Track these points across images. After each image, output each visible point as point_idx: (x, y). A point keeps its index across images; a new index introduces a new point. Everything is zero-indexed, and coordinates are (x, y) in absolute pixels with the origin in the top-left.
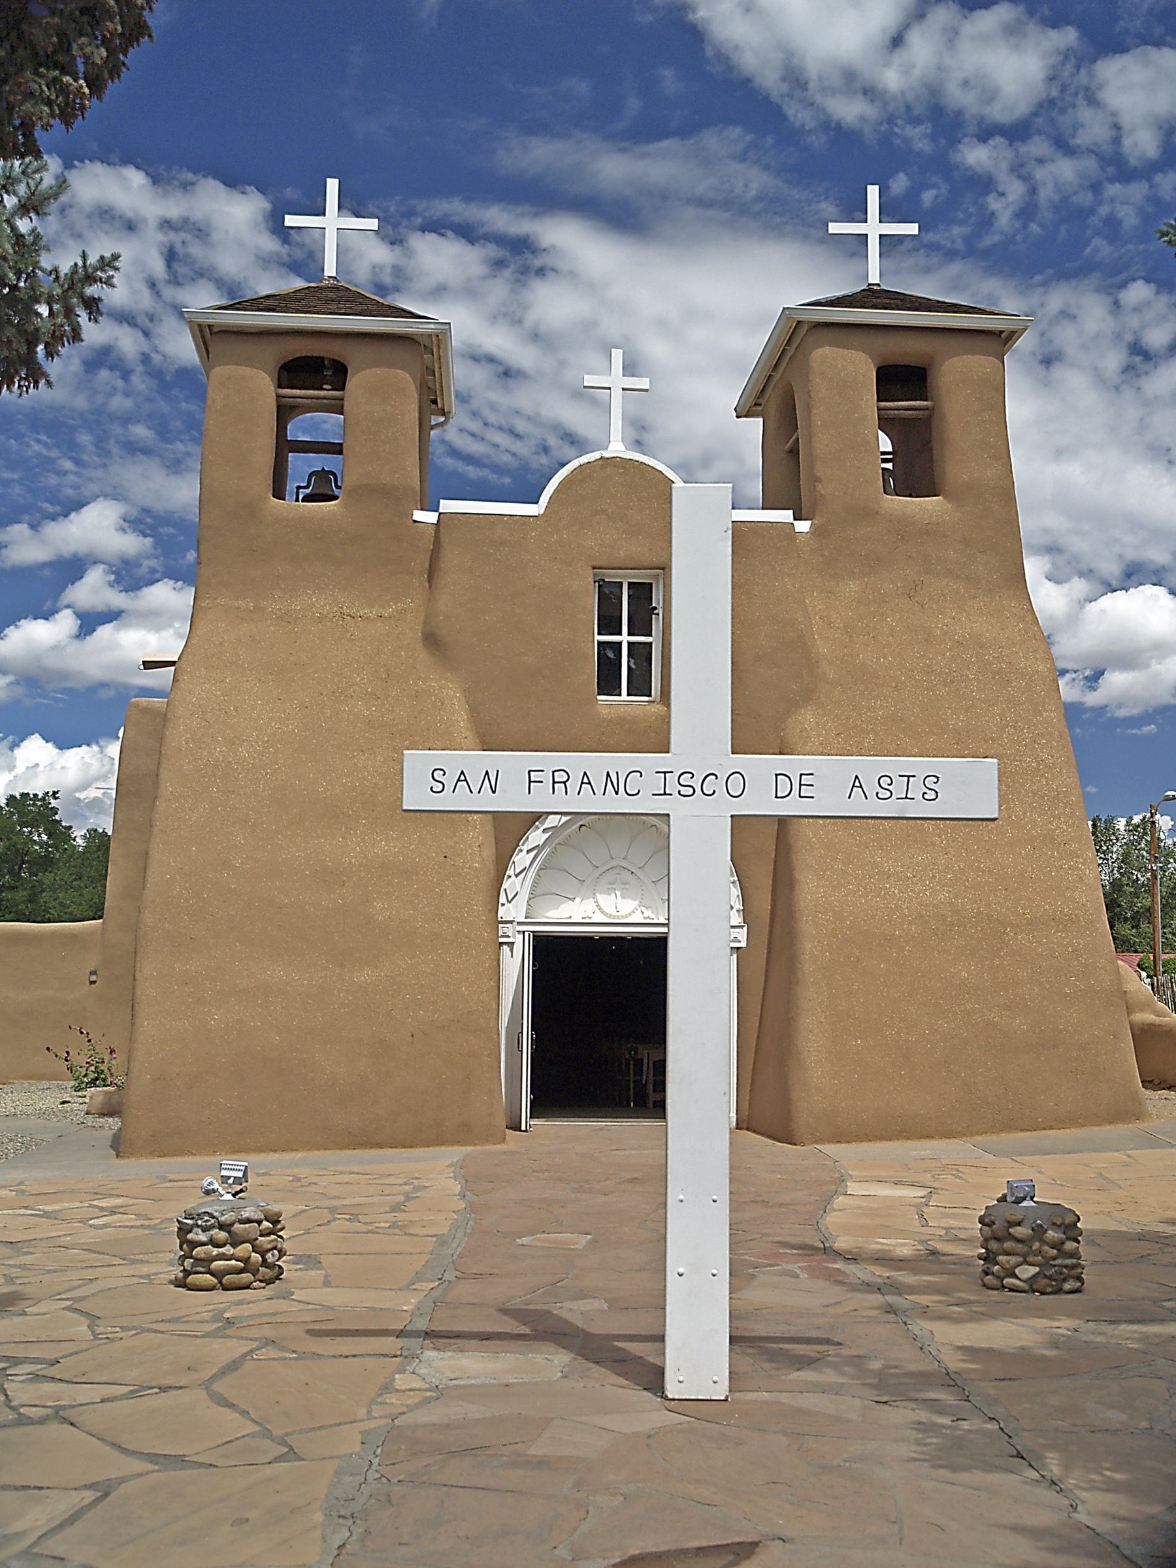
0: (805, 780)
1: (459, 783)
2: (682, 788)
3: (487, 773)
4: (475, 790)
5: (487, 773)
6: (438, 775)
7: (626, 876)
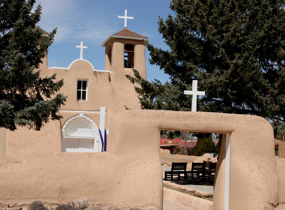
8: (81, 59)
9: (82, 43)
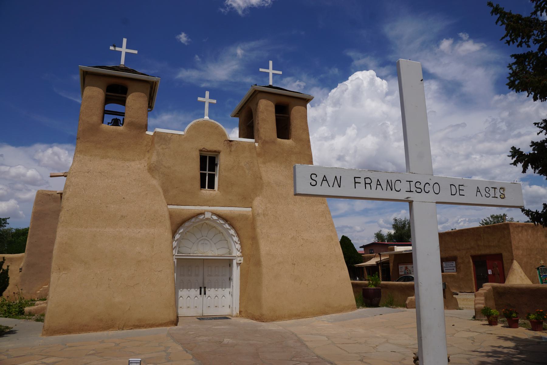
0: (461, 188)
1: (323, 181)
2: (417, 189)
3: (336, 177)
4: (331, 185)
5: (336, 177)
6: (313, 177)
7: (207, 242)
8: (206, 118)
9: (207, 94)
